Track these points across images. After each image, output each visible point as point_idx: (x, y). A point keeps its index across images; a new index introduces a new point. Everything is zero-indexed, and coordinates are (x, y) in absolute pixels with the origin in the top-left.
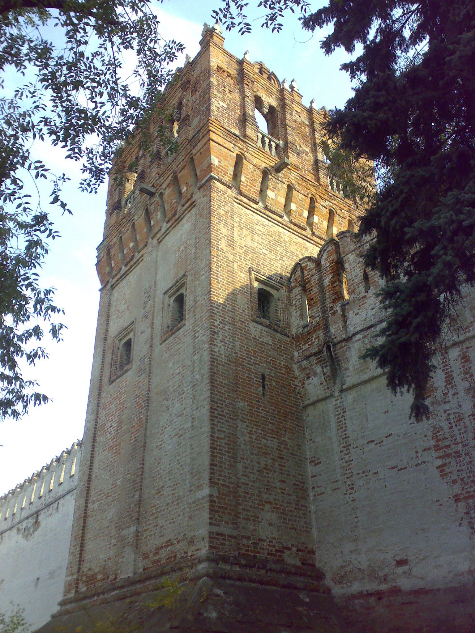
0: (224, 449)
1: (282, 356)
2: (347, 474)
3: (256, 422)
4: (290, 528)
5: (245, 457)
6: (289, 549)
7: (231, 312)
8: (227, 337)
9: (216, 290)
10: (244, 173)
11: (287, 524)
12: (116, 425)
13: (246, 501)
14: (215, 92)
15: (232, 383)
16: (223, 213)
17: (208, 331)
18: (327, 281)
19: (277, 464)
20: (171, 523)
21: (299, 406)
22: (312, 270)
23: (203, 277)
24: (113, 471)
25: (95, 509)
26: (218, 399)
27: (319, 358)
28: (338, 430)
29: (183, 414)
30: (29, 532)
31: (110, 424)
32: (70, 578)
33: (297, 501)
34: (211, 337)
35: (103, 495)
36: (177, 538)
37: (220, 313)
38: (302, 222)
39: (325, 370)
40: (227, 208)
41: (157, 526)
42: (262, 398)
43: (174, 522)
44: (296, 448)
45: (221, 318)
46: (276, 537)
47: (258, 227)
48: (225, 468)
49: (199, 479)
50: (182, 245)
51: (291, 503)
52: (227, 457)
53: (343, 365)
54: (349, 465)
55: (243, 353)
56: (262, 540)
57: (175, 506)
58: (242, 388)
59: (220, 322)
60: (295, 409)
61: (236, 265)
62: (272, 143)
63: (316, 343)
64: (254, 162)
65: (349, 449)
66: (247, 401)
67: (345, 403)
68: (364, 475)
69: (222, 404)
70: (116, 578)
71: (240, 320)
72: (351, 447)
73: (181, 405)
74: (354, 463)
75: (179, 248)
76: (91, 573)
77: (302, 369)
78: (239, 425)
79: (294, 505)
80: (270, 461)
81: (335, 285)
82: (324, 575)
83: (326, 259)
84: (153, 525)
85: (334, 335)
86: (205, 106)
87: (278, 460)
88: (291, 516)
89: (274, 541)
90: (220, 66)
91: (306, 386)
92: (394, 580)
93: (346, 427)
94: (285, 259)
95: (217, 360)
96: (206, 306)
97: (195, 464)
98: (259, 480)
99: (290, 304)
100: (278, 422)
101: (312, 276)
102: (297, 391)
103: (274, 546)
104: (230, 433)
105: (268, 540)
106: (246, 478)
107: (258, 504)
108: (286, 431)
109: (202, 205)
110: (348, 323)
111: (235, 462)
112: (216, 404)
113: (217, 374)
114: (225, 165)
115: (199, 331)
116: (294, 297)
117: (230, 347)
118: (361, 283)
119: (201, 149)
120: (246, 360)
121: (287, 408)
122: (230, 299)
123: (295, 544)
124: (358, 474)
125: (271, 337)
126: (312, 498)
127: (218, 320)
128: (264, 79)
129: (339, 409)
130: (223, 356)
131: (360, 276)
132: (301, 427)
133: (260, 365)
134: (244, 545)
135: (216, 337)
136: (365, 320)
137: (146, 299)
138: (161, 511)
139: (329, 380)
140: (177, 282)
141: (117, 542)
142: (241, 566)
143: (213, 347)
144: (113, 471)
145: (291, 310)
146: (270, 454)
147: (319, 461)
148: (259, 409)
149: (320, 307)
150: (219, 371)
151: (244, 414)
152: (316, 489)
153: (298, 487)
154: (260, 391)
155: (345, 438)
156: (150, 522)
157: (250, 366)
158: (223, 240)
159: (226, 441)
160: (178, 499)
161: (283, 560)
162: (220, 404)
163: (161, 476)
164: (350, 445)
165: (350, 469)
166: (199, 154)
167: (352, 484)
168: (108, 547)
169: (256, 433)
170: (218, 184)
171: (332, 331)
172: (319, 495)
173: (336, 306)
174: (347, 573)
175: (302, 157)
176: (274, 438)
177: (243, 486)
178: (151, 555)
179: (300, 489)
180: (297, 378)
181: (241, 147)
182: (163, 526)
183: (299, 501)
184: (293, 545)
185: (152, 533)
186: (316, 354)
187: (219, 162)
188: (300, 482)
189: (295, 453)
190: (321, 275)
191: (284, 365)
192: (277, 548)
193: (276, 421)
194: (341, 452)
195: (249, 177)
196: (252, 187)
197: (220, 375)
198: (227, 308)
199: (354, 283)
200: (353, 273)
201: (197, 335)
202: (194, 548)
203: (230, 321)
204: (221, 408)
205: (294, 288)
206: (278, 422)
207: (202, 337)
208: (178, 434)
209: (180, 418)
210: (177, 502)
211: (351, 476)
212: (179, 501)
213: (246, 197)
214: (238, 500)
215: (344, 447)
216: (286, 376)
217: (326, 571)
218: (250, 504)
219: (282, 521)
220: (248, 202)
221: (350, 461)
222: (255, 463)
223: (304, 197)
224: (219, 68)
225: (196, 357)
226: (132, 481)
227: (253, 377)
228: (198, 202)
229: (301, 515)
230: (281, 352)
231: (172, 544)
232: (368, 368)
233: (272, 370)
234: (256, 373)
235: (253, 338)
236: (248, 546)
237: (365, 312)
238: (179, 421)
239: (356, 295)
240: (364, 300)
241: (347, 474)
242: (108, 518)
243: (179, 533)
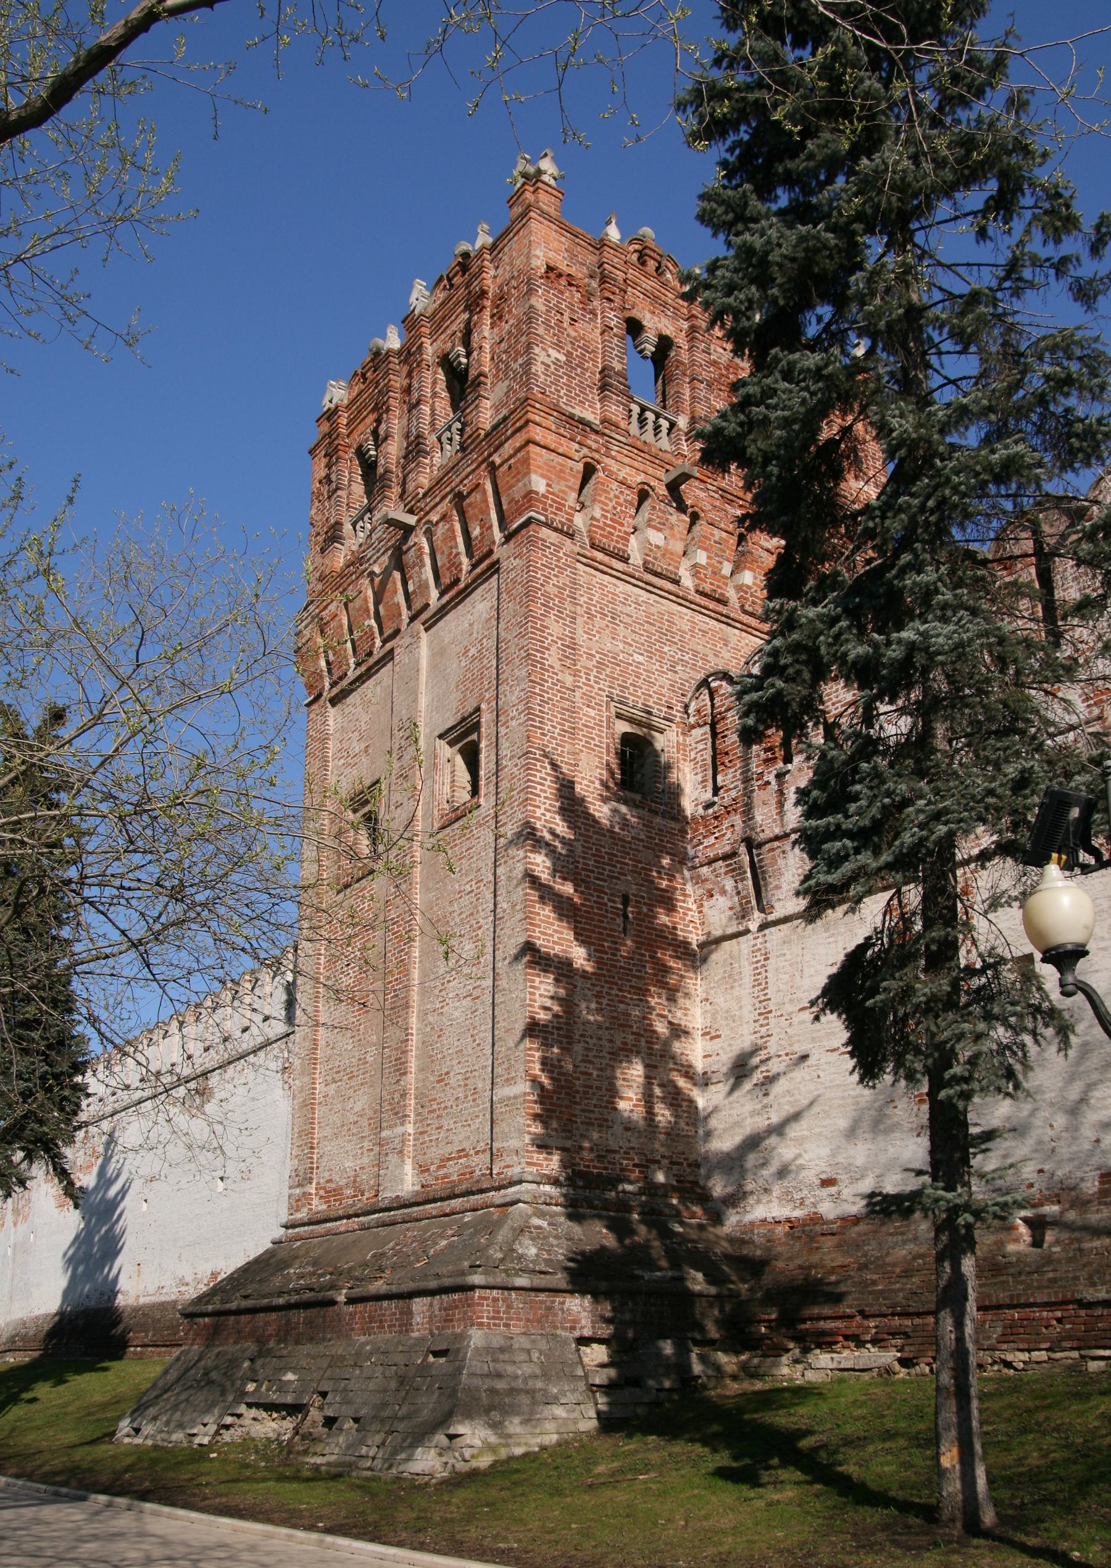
14: (541, 331)
16: (552, 590)
19: (643, 1040)
23: (514, 723)
39: (815, 793)
40: (564, 580)
47: (627, 610)
56: (614, 1152)
61: (578, 694)
62: (662, 421)
63: (728, 835)
64: (621, 475)
86: (520, 361)
90: (552, 264)
91: (705, 910)
92: (814, 1205)
94: (679, 668)
102: (688, 918)
109: (512, 575)
111: (569, 1043)
119: (511, 457)
128: (647, 275)
137: (403, 743)
140: (463, 719)
158: (553, 648)
166: (506, 466)
169: (609, 994)
170: (545, 532)
171: (758, 818)
177: (582, 1077)
178: (433, 1168)
181: (594, 446)
184: (663, 1157)
186: (725, 857)
187: (548, 485)
195: (609, 508)
213: (603, 550)
218: (594, 1102)
220: (606, 559)
222: (605, 1043)
223: (724, 535)
224: (550, 269)
228: (504, 565)
231: (466, 1156)
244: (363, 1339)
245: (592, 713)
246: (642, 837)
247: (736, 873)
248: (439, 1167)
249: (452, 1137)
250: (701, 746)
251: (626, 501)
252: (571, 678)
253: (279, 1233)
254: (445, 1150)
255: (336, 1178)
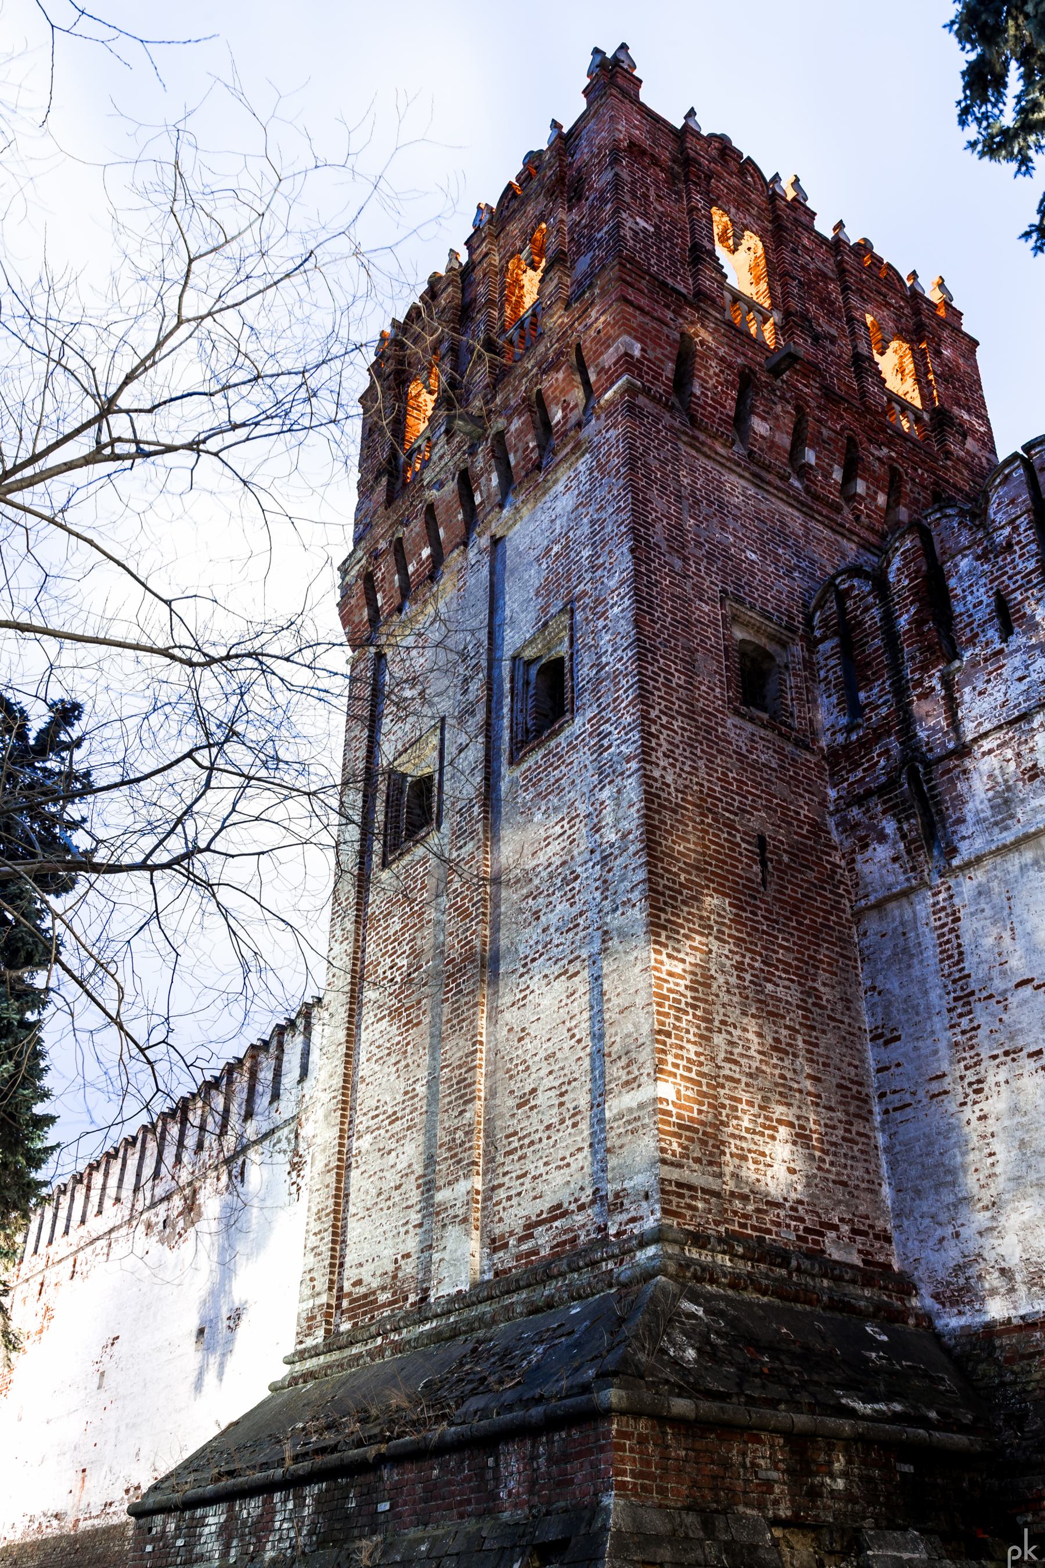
0: (683, 1000)
1: (803, 796)
2: (964, 1059)
3: (751, 943)
4: (834, 1182)
5: (730, 1021)
6: (835, 1228)
7: (686, 689)
8: (678, 747)
9: (649, 638)
10: (700, 377)
11: (828, 1171)
12: (405, 962)
13: (737, 1118)
15: (694, 851)
17: (635, 732)
18: (903, 622)
19: (799, 1038)
20: (559, 1167)
21: (844, 911)
22: (865, 597)
23: (616, 610)
24: (403, 1063)
25: (363, 1151)
26: (665, 886)
27: (890, 799)
28: (942, 961)
29: (578, 925)
30: (174, 1229)
31: (388, 960)
32: (310, 1304)
33: (846, 1123)
34: (642, 745)
35: (381, 1117)
36: (576, 1200)
37: (659, 690)
38: (830, 493)
41: (524, 1175)
42: (762, 889)
43: (568, 1165)
44: (839, 1006)
45: (664, 703)
46: (806, 1199)
48: (688, 1041)
49: (628, 1066)
50: (556, 542)
51: (834, 1127)
52: (690, 1018)
53: (951, 811)
54: (971, 1038)
55: (716, 785)
57: (570, 1130)
58: (716, 866)
59: (661, 711)
60: (833, 918)
63: (882, 763)
65: (969, 1003)
66: (728, 896)
67: (956, 900)
68: (1009, 1059)
69: (676, 899)
70: (424, 1299)
71: (704, 710)
72: (976, 997)
73: (571, 905)
74: (982, 1033)
75: (548, 550)
76: (362, 1290)
77: (848, 827)
78: (714, 949)
79: (841, 1132)
80: (785, 1032)
81: (926, 629)
82: (915, 1287)
83: (898, 569)
84: (514, 1175)
85: (927, 744)
87: (803, 1030)
88: (835, 1154)
89: (800, 1208)
91: (858, 866)
93: (961, 953)
95: (659, 797)
96: (626, 675)
97: (616, 1034)
98: (764, 1072)
99: (814, 678)
100: (800, 946)
101: (866, 609)
103: (802, 1220)
104: (696, 965)
105: (787, 1205)
106: (734, 1067)
107: (764, 1126)
108: (817, 968)
110: (960, 714)
112: (662, 899)
113: (660, 829)
114: (656, 358)
115: (610, 733)
116: (822, 663)
117: (687, 768)
118: (991, 620)
120: (721, 801)
121: (818, 916)
122: (681, 660)
123: (847, 1216)
124: (994, 1057)
125: (775, 751)
126: (879, 1118)
127: (657, 707)
129: (943, 914)
130: (672, 790)
131: (988, 605)
132: (849, 959)
133: (752, 815)
134: (735, 1213)
135: (653, 745)
136: (1003, 705)
138: (532, 1143)
139: (917, 849)
141: (424, 1217)
142: (733, 1256)
143: (648, 767)
144: (403, 1063)
145: (817, 692)
146: (784, 1017)
147: (895, 1034)
148: (755, 914)
149: (888, 683)
150: (665, 824)
151: (723, 924)
152: (890, 1097)
153: (849, 1093)
154: (756, 875)
155: (960, 979)
156: (506, 1169)
157: (732, 817)
158: (658, 526)
159: (688, 983)
160: (574, 1115)
161: (823, 1252)
162: (670, 897)
163: (528, 1068)
164: (972, 993)
165: (972, 1047)
167: (979, 1081)
168: (403, 1230)
169: (752, 967)
172: (895, 1109)
173: (930, 677)
174: (972, 1281)
175: (824, 347)
176: (792, 981)
178: (512, 1242)
179: (853, 1097)
180: (835, 848)
182: (541, 1175)
183: (851, 1124)
184: (842, 1220)
185: (513, 1192)
186: (882, 790)
187: (643, 350)
188: (852, 1082)
189: (838, 1016)
190: (889, 608)
191: (806, 816)
192: (808, 1224)
193: (795, 944)
194: (950, 1010)
195: (709, 386)
196: (716, 409)
197: (666, 831)
198: (675, 680)
199: (972, 623)
200: (969, 598)
201: (606, 743)
202: (625, 1217)
203: (684, 711)
204: (673, 907)
205: (822, 640)
206: (800, 946)
207: (618, 746)
208: (566, 972)
209: (571, 934)
210: (573, 1120)
211: (976, 1064)
212: (578, 1118)
214: (720, 1114)
215: (956, 999)
216: (812, 843)
217: (920, 1280)
219: (816, 1165)
221: (974, 1029)
224: (632, 144)
225: (606, 794)
226: (455, 1081)
227: (738, 840)
229: (857, 1154)
230: (798, 787)
231: (565, 1214)
232: (1012, 816)
233: (779, 826)
234: (745, 833)
235: (735, 752)
236: (746, 1216)
237: (1003, 688)
238: (568, 943)
239: (977, 651)
240: (999, 660)
241: (964, 1059)
242: (399, 1167)
243: (582, 1189)
244: (413, 1533)
245: (706, 608)
246: (774, 766)
247: (898, 811)
248: (521, 1240)
249: (541, 1187)
250: (833, 662)
251: (726, 380)
252: (680, 563)
253: (281, 1372)
254: (531, 1209)
255: (367, 1278)
